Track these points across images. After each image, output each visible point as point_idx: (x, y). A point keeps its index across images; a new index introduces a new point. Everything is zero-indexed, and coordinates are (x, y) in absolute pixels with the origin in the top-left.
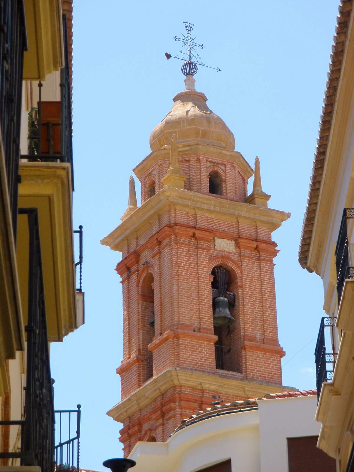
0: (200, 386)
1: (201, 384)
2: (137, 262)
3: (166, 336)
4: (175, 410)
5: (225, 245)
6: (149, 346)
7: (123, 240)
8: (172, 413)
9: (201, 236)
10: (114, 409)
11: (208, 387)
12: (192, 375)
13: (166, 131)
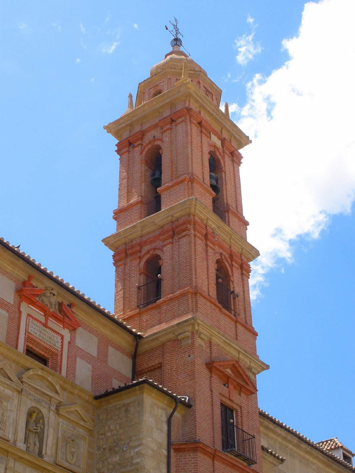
0: (206, 221)
1: (207, 220)
2: (142, 139)
3: (183, 178)
4: (189, 230)
5: (216, 140)
6: (158, 189)
7: (127, 126)
8: (186, 232)
9: (205, 125)
10: (113, 235)
11: (211, 225)
12: (204, 209)
13: (170, 63)
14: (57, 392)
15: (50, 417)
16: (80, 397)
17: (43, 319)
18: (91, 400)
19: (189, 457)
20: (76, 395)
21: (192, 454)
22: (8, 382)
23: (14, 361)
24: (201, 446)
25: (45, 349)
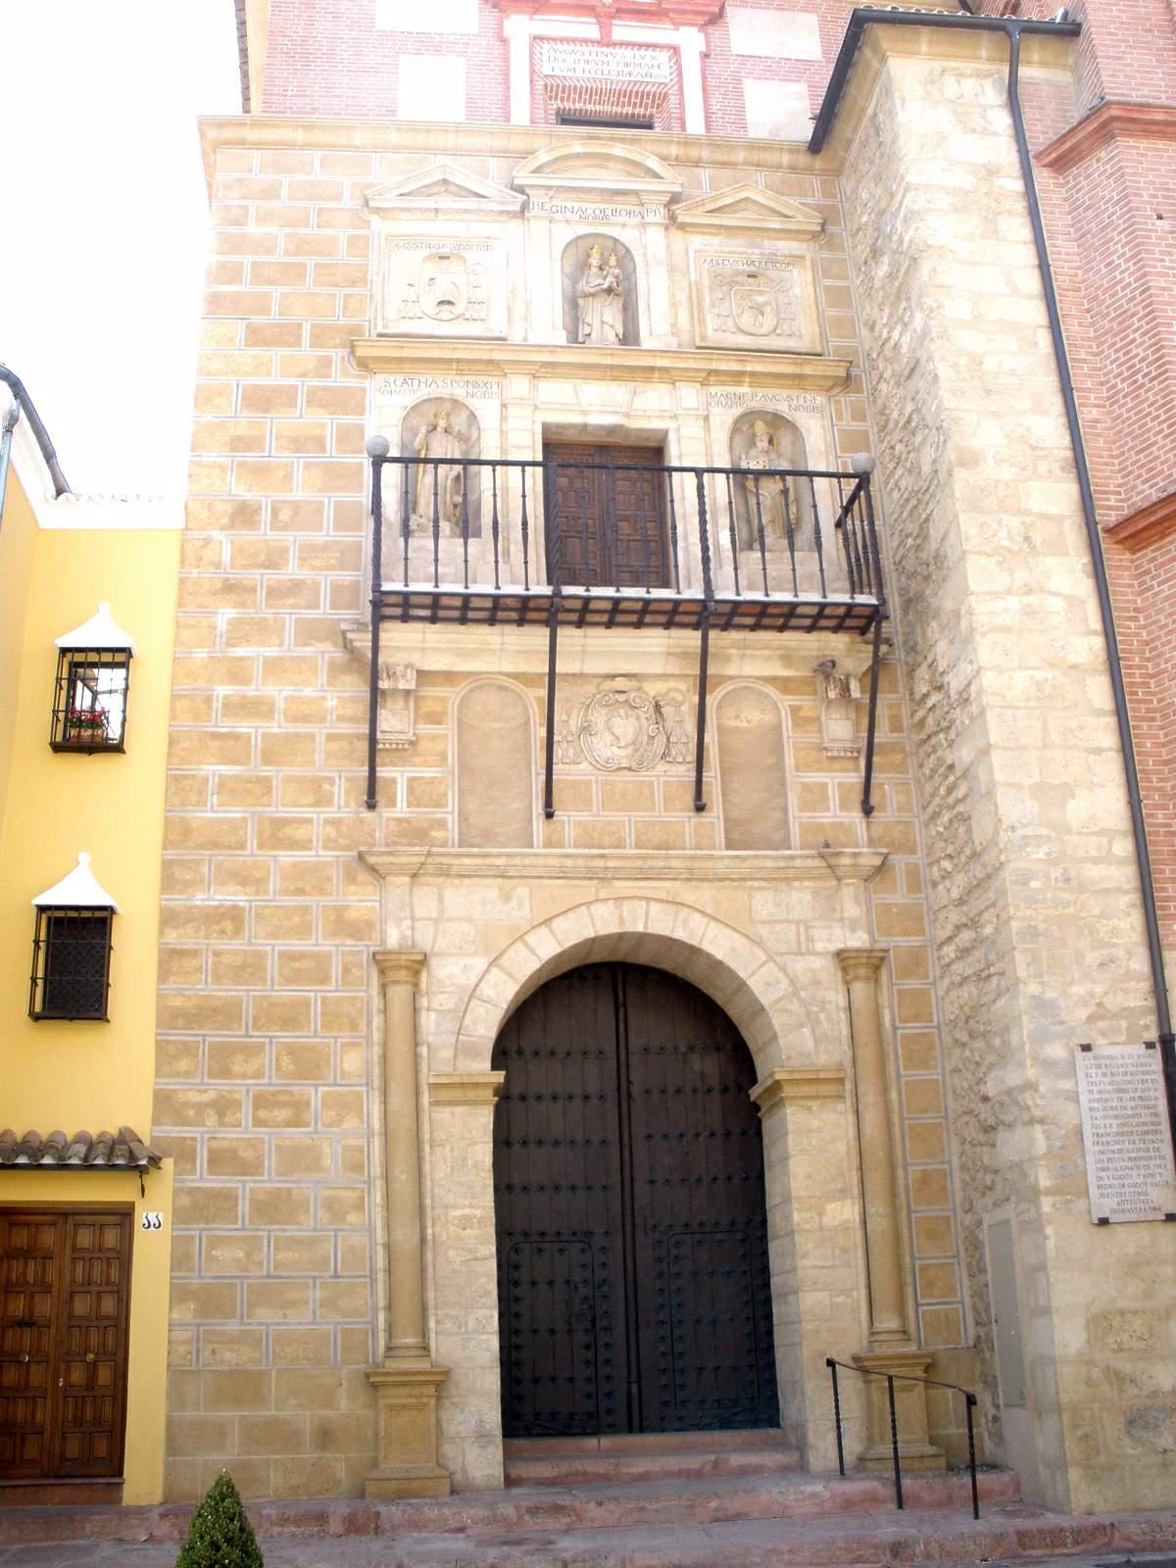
14: (657, 176)
15: (650, 246)
16: (758, 165)
17: (592, 31)
18: (803, 159)
19: (1099, 166)
20: (744, 164)
21: (1103, 154)
22: (472, 203)
23: (493, 153)
24: (1115, 112)
25: (622, 94)
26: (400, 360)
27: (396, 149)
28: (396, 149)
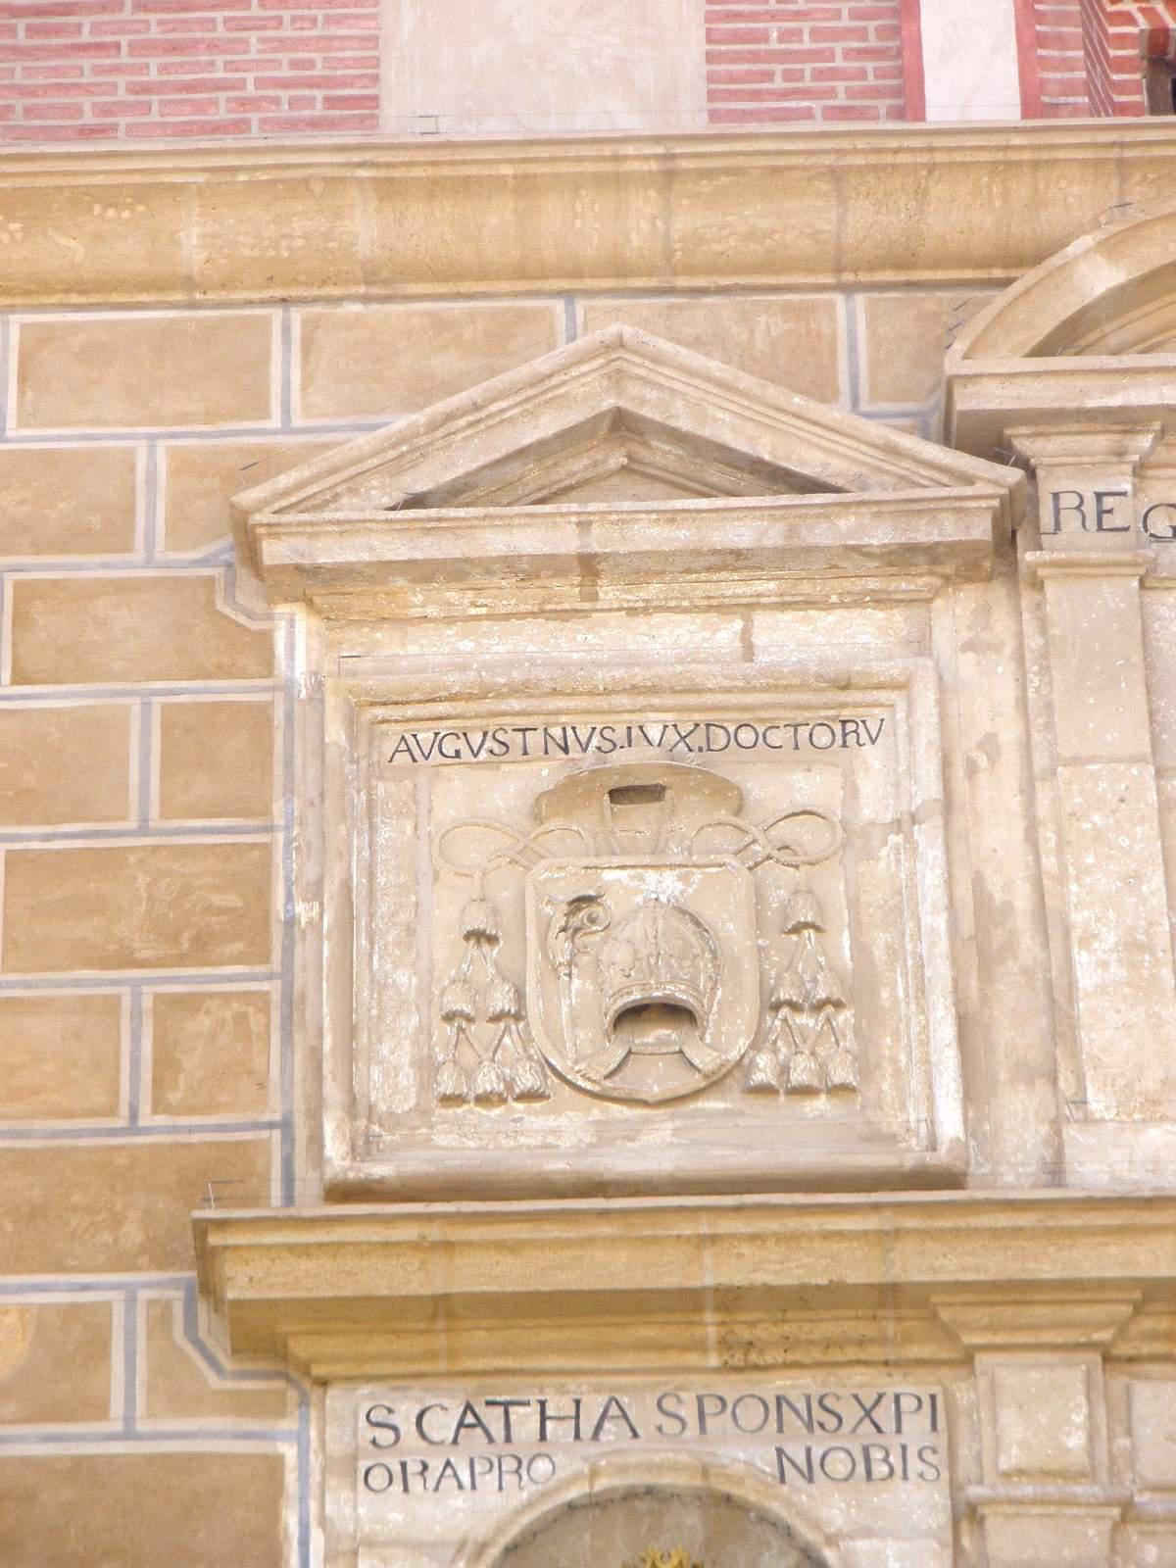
22: (746, 523)
26: (443, 1309)
27: (383, 281)
28: (383, 281)
